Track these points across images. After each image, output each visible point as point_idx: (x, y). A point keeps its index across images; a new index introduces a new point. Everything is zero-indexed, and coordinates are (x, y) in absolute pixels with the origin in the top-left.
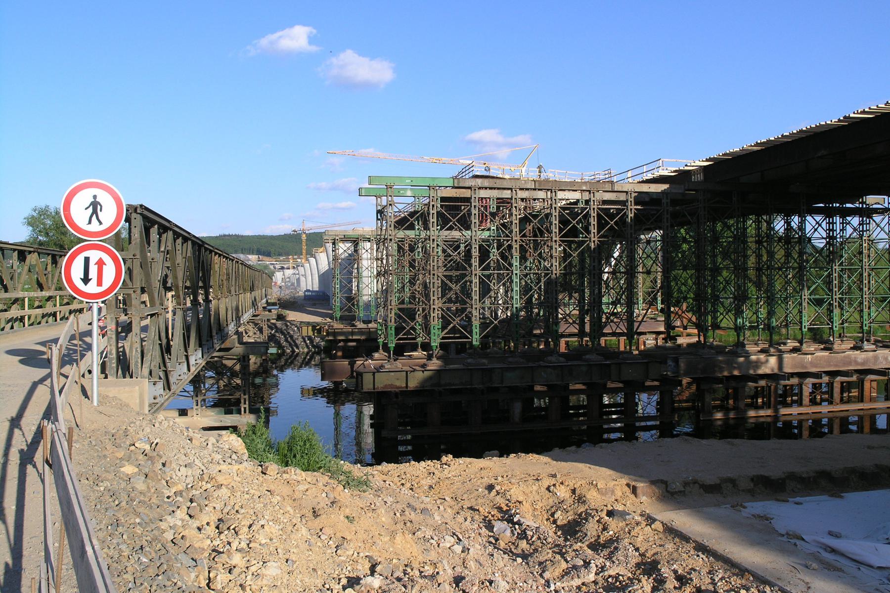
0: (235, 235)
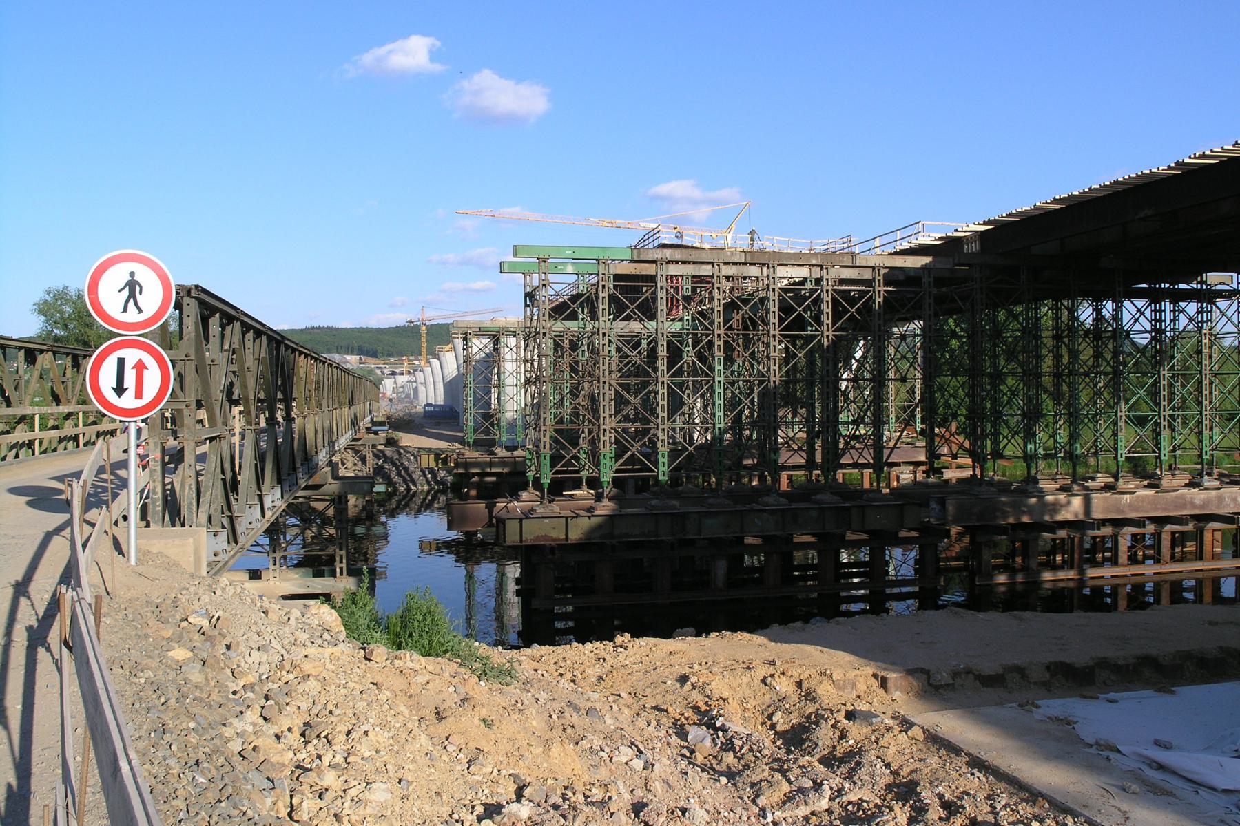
0: (328, 328)
